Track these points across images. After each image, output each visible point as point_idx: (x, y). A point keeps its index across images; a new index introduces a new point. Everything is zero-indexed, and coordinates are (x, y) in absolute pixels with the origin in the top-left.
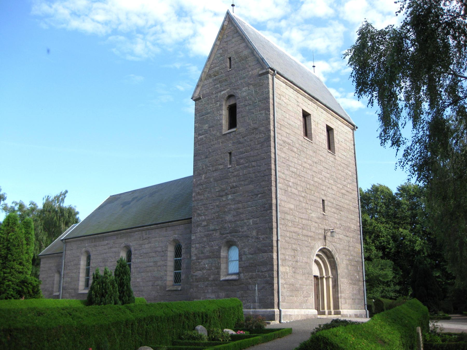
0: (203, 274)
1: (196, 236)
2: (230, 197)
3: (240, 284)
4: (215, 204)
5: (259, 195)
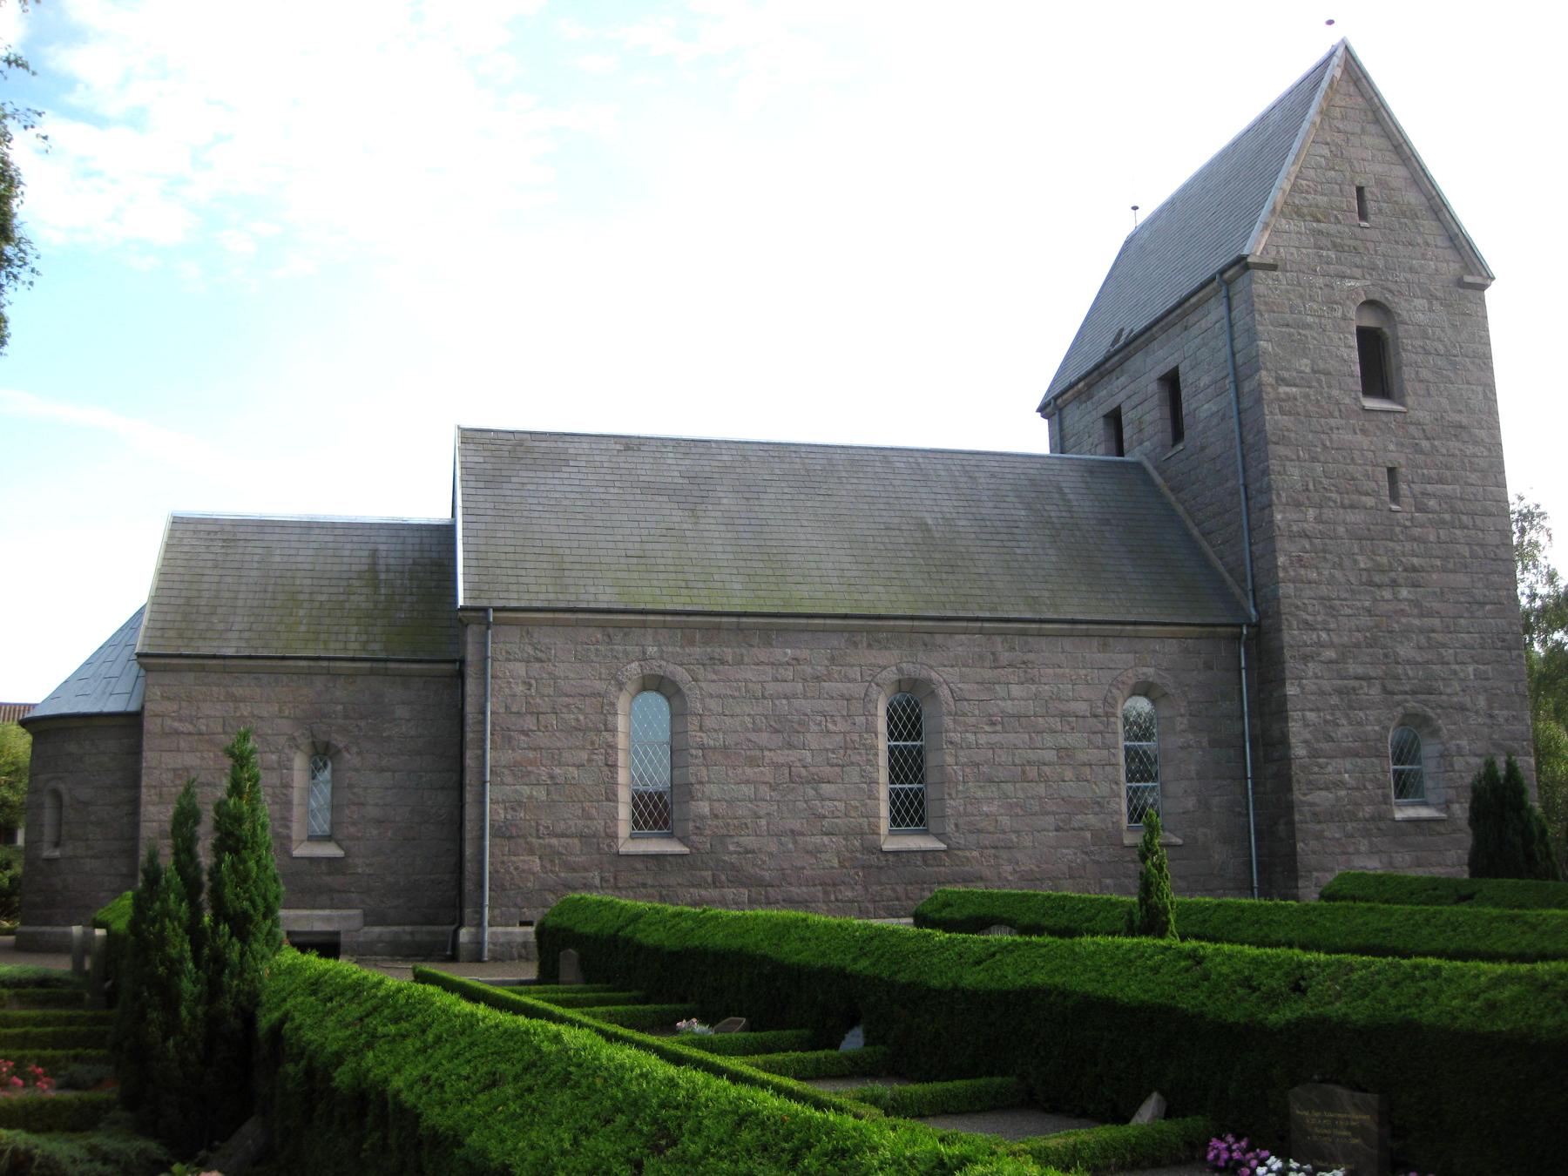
0: (1338, 799)
1: (1302, 687)
2: (1404, 593)
3: (1454, 831)
4: (1359, 604)
5: (1488, 607)
